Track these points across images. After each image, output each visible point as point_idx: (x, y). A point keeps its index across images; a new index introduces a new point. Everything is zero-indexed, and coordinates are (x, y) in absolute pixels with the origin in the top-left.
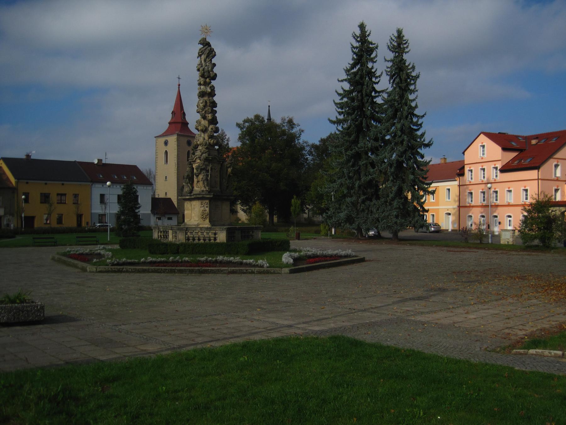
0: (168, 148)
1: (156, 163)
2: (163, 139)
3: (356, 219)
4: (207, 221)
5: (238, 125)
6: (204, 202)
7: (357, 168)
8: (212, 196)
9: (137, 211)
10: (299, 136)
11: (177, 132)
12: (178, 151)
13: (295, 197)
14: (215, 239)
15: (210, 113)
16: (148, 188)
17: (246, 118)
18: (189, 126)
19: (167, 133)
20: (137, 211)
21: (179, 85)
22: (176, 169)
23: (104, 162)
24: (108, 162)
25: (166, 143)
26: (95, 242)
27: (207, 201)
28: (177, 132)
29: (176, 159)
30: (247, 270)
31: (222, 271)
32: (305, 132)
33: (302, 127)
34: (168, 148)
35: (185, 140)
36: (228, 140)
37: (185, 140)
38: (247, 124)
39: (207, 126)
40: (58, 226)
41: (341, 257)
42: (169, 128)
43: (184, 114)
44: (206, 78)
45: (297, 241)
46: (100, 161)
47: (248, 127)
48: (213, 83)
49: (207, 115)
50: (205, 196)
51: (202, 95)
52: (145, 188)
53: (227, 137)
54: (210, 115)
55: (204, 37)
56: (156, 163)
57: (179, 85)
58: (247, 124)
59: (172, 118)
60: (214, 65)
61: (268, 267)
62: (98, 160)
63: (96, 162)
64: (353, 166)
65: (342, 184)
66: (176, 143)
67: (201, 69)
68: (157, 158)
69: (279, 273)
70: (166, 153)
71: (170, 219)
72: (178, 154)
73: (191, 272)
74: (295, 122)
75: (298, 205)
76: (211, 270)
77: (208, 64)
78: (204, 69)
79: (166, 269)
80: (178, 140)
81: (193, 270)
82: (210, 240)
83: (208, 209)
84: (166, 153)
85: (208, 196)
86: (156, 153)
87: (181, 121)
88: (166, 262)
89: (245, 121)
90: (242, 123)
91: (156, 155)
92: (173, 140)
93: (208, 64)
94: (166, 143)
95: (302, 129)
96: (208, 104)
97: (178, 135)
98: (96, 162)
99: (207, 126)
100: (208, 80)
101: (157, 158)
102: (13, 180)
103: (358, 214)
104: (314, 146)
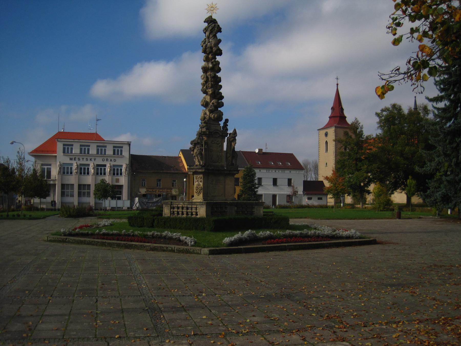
1: (319, 151)
2: (324, 131)
3: (452, 198)
4: (201, 195)
5: (377, 114)
6: (199, 176)
7: (455, 145)
8: (203, 170)
9: (256, 190)
11: (335, 125)
13: (410, 177)
14: (197, 215)
15: (211, 87)
16: (300, 172)
18: (347, 119)
19: (328, 126)
20: (256, 190)
21: (337, 85)
22: (334, 156)
23: (264, 151)
24: (268, 151)
25: (326, 135)
27: (201, 176)
28: (335, 125)
29: (334, 148)
30: (167, 248)
31: (144, 247)
36: (362, 128)
38: (385, 113)
39: (209, 101)
40: (288, 204)
41: (341, 237)
42: (329, 121)
43: (342, 109)
44: (209, 54)
45: (398, 220)
46: (260, 150)
47: (387, 116)
48: (218, 58)
49: (208, 90)
50: (198, 170)
51: (205, 70)
52: (298, 172)
53: (361, 125)
54: (210, 90)
55: (210, 15)
56: (319, 151)
57: (337, 85)
58: (385, 113)
59: (332, 113)
60: (220, 41)
61: (192, 246)
62: (259, 150)
63: (257, 151)
64: (450, 143)
65: (440, 162)
66: (334, 134)
67: (204, 46)
68: (319, 147)
69: (198, 253)
73: (103, 244)
75: (412, 185)
76: (135, 245)
77: (211, 40)
78: (206, 45)
79: (98, 242)
80: (336, 131)
81: (119, 244)
82: (192, 214)
83: (201, 184)
85: (200, 171)
86: (319, 143)
88: (119, 235)
89: (382, 111)
90: (380, 112)
91: (319, 145)
92: (331, 131)
93: (211, 40)
94: (326, 135)
96: (210, 79)
97: (336, 127)
98: (257, 151)
99: (209, 101)
100: (210, 56)
101: (319, 147)
102: (186, 167)
103: (456, 193)
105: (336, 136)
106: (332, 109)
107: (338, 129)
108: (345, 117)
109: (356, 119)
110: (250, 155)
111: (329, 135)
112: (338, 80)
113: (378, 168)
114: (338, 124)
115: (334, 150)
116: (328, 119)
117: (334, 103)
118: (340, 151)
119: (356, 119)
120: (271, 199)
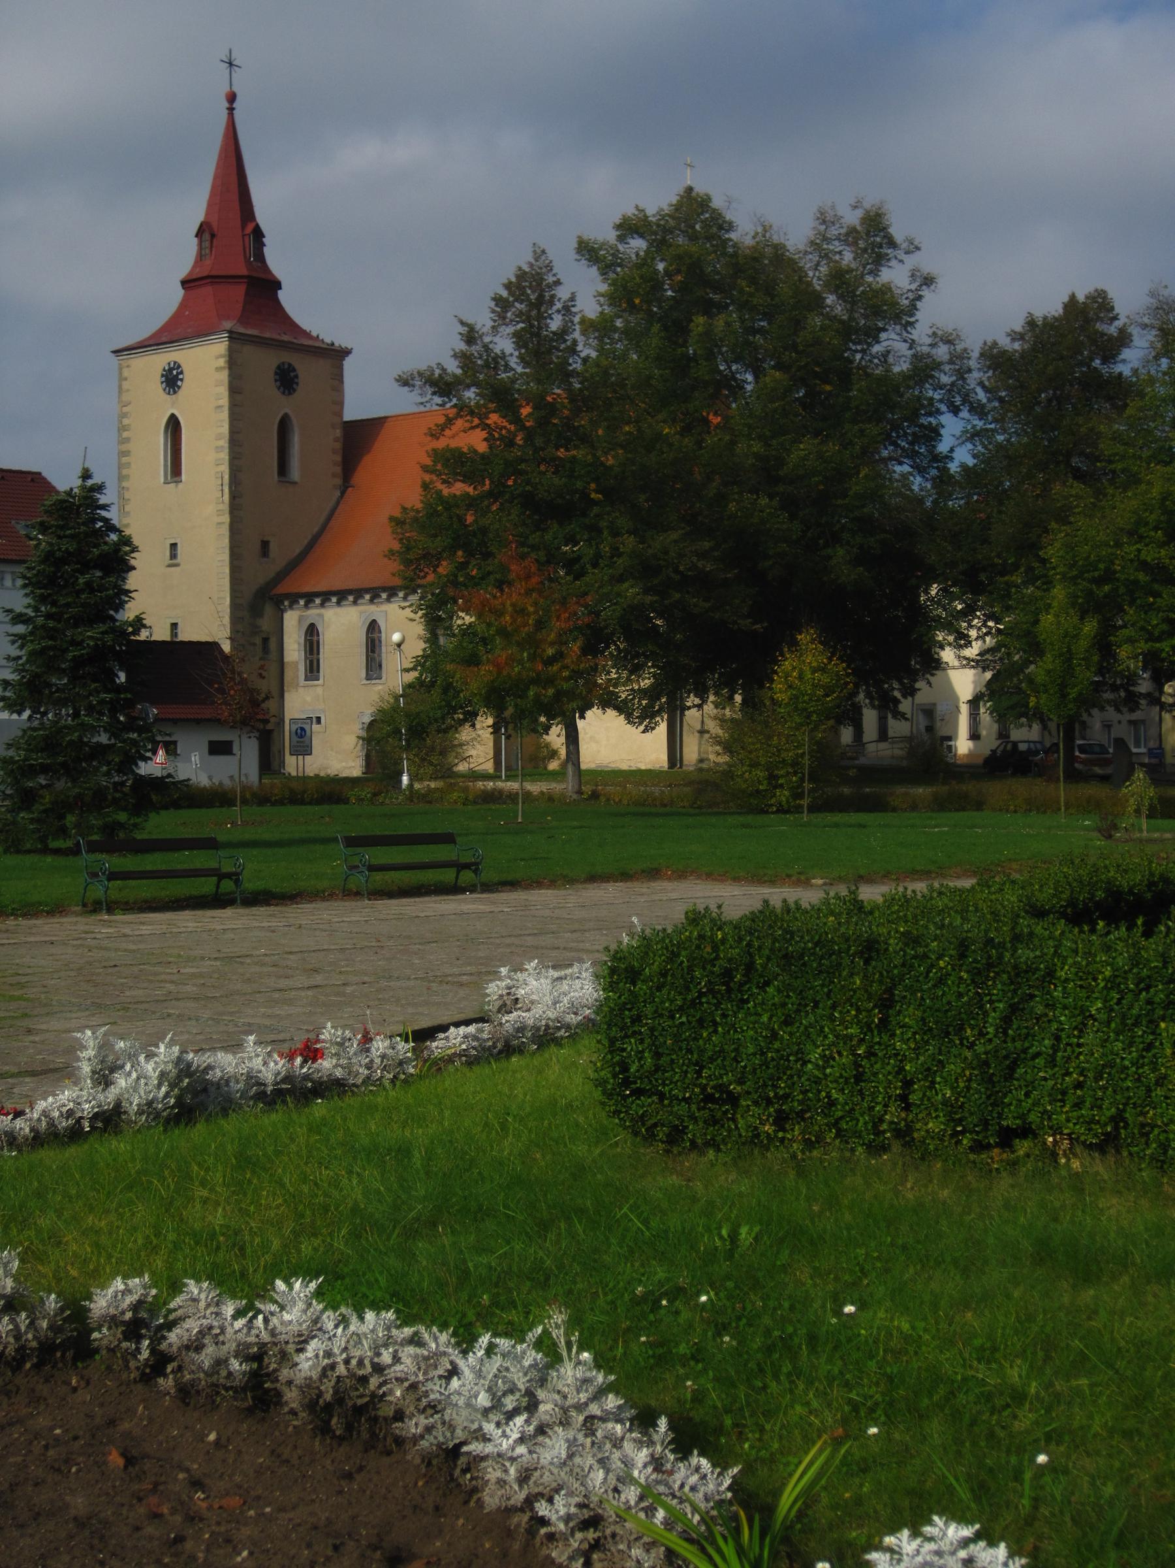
0: (184, 405)
2: (159, 360)
10: (912, 309)
11: (228, 325)
12: (234, 418)
17: (630, 211)
18: (281, 295)
21: (232, 98)
22: (226, 507)
25: (172, 380)
26: (448, 875)
28: (228, 325)
29: (225, 456)
32: (941, 283)
33: (925, 262)
34: (184, 405)
35: (269, 361)
37: (269, 361)
42: (183, 305)
43: (258, 234)
53: (563, 293)
57: (232, 98)
58: (638, 244)
59: (200, 257)
66: (224, 376)
70: (174, 426)
71: (219, 749)
72: (233, 432)
74: (898, 232)
75: (1083, 644)
80: (233, 362)
84: (174, 426)
87: (244, 272)
89: (629, 228)
92: (206, 362)
94: (172, 380)
95: (927, 268)
97: (233, 337)
104: (995, 358)
105: (341, 368)
106: (199, 234)
107: (248, 350)
108: (277, 285)
109: (540, 254)
110: (604, 272)
111: (188, 385)
112: (237, 74)
113: (529, 592)
114: (243, 320)
115: (225, 468)
116: (179, 293)
117: (210, 205)
118: (441, 444)
119: (540, 254)
120: (948, 734)
